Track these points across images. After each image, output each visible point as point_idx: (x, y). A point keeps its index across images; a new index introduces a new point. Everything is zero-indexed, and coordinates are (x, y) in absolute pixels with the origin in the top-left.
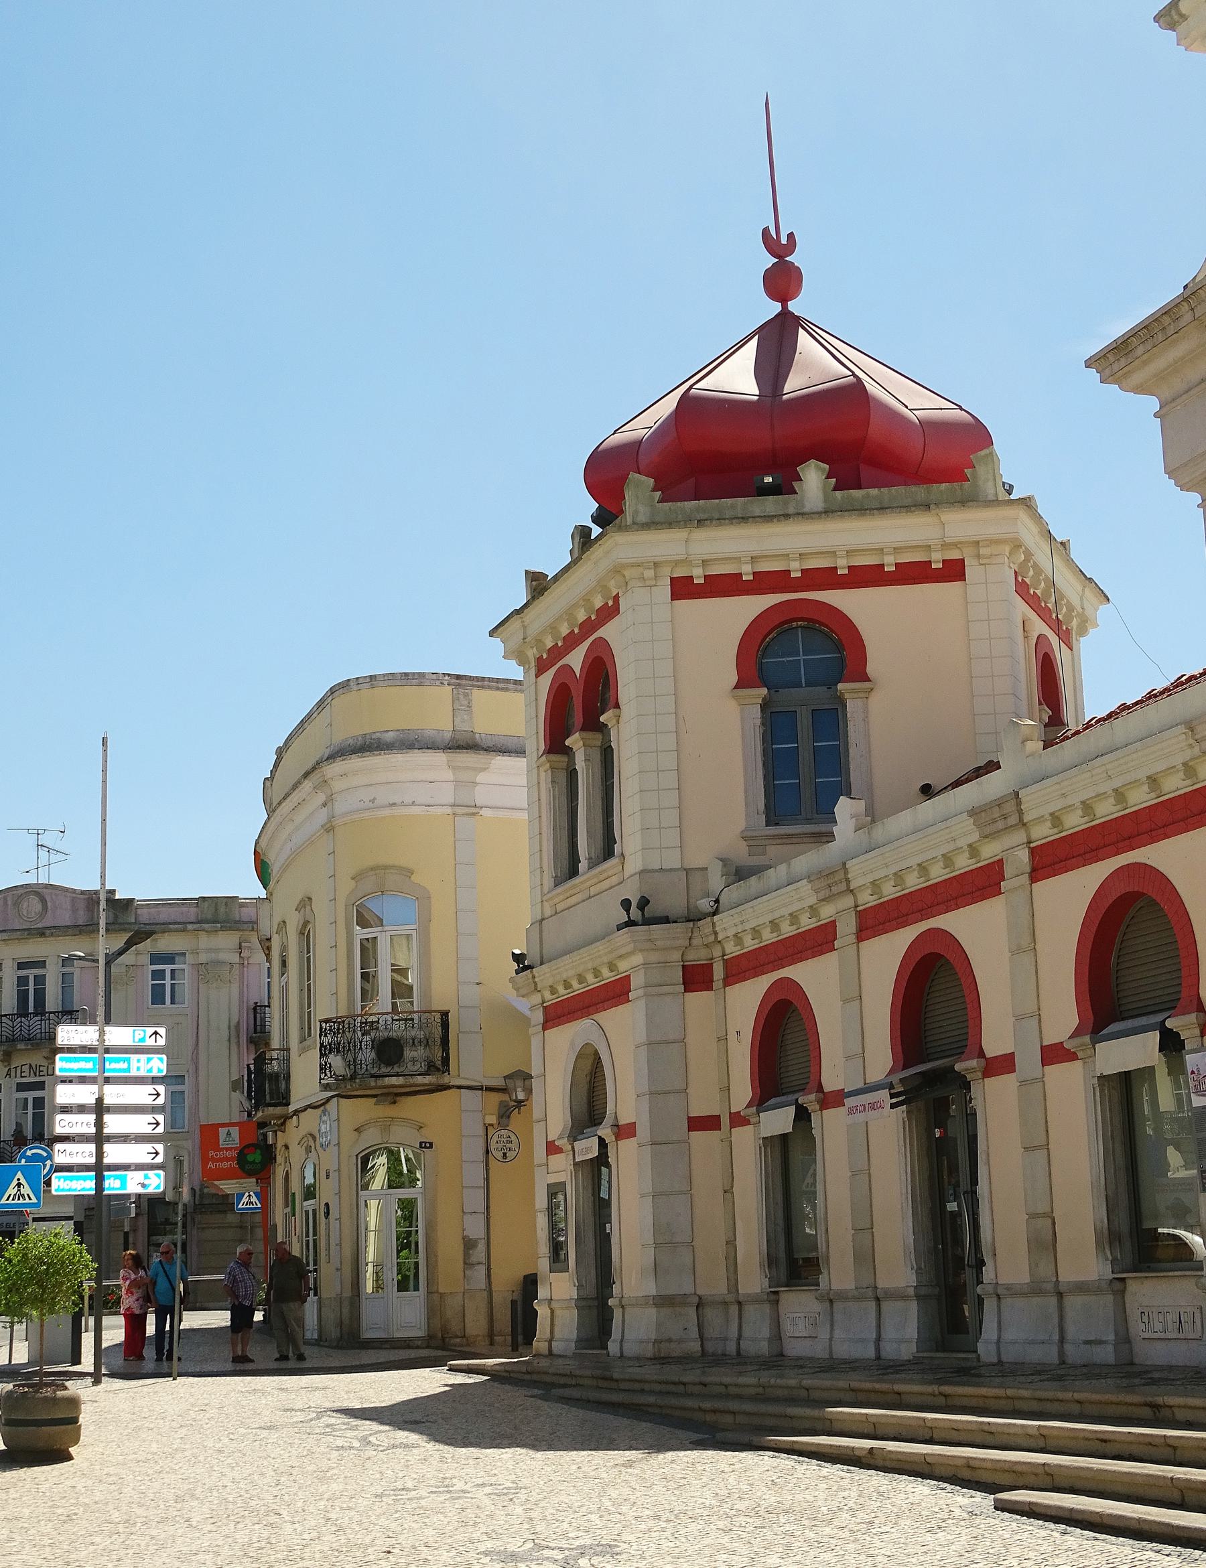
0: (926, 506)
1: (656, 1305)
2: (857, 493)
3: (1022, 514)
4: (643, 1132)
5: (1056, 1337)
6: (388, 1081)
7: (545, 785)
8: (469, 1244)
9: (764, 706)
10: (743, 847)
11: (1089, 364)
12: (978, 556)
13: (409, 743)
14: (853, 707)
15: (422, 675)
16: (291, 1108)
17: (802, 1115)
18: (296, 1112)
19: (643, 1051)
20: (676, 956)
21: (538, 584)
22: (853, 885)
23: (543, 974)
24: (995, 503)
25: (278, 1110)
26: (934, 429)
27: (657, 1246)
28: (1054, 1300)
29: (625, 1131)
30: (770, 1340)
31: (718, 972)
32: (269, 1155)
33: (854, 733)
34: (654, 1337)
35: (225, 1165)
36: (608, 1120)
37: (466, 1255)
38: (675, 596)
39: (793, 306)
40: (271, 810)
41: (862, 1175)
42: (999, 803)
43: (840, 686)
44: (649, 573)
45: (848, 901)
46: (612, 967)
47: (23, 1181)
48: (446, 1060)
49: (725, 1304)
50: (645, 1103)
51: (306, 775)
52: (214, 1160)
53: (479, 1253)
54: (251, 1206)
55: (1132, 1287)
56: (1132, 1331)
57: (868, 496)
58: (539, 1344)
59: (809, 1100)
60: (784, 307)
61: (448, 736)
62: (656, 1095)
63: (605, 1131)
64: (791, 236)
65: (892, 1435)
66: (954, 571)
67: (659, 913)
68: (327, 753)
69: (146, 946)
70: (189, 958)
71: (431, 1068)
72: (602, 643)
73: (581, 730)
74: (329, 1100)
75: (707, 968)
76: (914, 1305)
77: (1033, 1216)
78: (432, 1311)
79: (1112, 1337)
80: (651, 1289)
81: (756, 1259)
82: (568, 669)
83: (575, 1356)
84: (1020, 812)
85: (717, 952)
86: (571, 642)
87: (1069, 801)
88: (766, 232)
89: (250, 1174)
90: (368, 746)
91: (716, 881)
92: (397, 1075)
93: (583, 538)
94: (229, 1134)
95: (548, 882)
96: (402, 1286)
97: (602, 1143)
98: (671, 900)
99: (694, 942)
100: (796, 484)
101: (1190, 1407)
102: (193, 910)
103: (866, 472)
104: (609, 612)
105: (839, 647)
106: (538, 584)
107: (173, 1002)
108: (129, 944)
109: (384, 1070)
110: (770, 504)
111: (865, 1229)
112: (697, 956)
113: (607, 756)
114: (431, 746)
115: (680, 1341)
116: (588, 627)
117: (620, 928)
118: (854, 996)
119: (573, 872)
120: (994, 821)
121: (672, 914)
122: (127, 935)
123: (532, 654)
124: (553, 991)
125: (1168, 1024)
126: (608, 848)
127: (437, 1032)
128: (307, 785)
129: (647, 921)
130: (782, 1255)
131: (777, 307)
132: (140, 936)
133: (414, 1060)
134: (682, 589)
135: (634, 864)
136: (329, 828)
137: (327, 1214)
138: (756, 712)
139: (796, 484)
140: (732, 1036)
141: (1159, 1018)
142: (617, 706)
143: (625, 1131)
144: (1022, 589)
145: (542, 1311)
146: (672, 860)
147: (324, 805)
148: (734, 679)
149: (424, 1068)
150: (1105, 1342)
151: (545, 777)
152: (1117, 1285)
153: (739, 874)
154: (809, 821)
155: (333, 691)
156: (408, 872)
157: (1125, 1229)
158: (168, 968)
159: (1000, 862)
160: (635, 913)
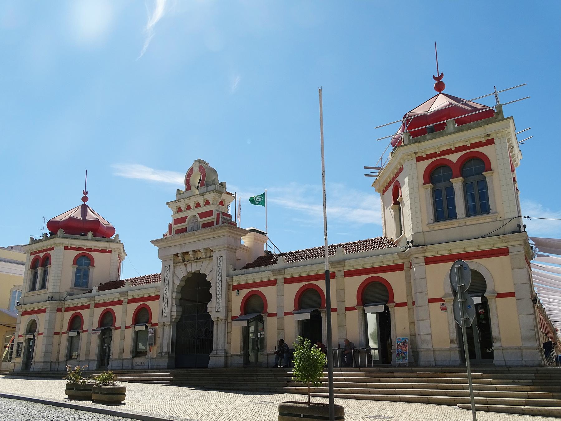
1: (43, 363)
3: (121, 245)
5: (122, 366)
11: (154, 242)
12: (114, 250)
17: (78, 333)
19: (48, 321)
20: (56, 306)
22: (95, 300)
26: (108, 228)
27: (45, 353)
28: (122, 361)
30: (131, 366)
31: (63, 309)
33: (90, 274)
34: (42, 368)
38: (65, 249)
39: (86, 203)
41: (89, 343)
43: (90, 267)
49: (55, 362)
50: (47, 330)
55: (135, 359)
56: (134, 364)
57: (98, 238)
59: (80, 331)
60: (85, 203)
64: (87, 192)
66: (110, 252)
73: (41, 267)
76: (96, 362)
79: (131, 365)
80: (43, 360)
87: (136, 294)
88: (84, 191)
97: (34, 336)
98: (57, 297)
100: (87, 235)
101: (516, 373)
110: (83, 237)
113: (45, 273)
115: (47, 369)
117: (46, 301)
118: (92, 316)
120: (123, 295)
121: (420, 245)
123: (30, 252)
126: (43, 286)
129: (52, 300)
130: (69, 354)
131: (83, 203)
134: (66, 248)
139: (87, 235)
140: (64, 320)
141: (145, 324)
144: (119, 256)
146: (58, 291)
150: (130, 366)
152: (133, 358)
153: (70, 294)
154: (81, 287)
157: (134, 351)
160: (50, 299)
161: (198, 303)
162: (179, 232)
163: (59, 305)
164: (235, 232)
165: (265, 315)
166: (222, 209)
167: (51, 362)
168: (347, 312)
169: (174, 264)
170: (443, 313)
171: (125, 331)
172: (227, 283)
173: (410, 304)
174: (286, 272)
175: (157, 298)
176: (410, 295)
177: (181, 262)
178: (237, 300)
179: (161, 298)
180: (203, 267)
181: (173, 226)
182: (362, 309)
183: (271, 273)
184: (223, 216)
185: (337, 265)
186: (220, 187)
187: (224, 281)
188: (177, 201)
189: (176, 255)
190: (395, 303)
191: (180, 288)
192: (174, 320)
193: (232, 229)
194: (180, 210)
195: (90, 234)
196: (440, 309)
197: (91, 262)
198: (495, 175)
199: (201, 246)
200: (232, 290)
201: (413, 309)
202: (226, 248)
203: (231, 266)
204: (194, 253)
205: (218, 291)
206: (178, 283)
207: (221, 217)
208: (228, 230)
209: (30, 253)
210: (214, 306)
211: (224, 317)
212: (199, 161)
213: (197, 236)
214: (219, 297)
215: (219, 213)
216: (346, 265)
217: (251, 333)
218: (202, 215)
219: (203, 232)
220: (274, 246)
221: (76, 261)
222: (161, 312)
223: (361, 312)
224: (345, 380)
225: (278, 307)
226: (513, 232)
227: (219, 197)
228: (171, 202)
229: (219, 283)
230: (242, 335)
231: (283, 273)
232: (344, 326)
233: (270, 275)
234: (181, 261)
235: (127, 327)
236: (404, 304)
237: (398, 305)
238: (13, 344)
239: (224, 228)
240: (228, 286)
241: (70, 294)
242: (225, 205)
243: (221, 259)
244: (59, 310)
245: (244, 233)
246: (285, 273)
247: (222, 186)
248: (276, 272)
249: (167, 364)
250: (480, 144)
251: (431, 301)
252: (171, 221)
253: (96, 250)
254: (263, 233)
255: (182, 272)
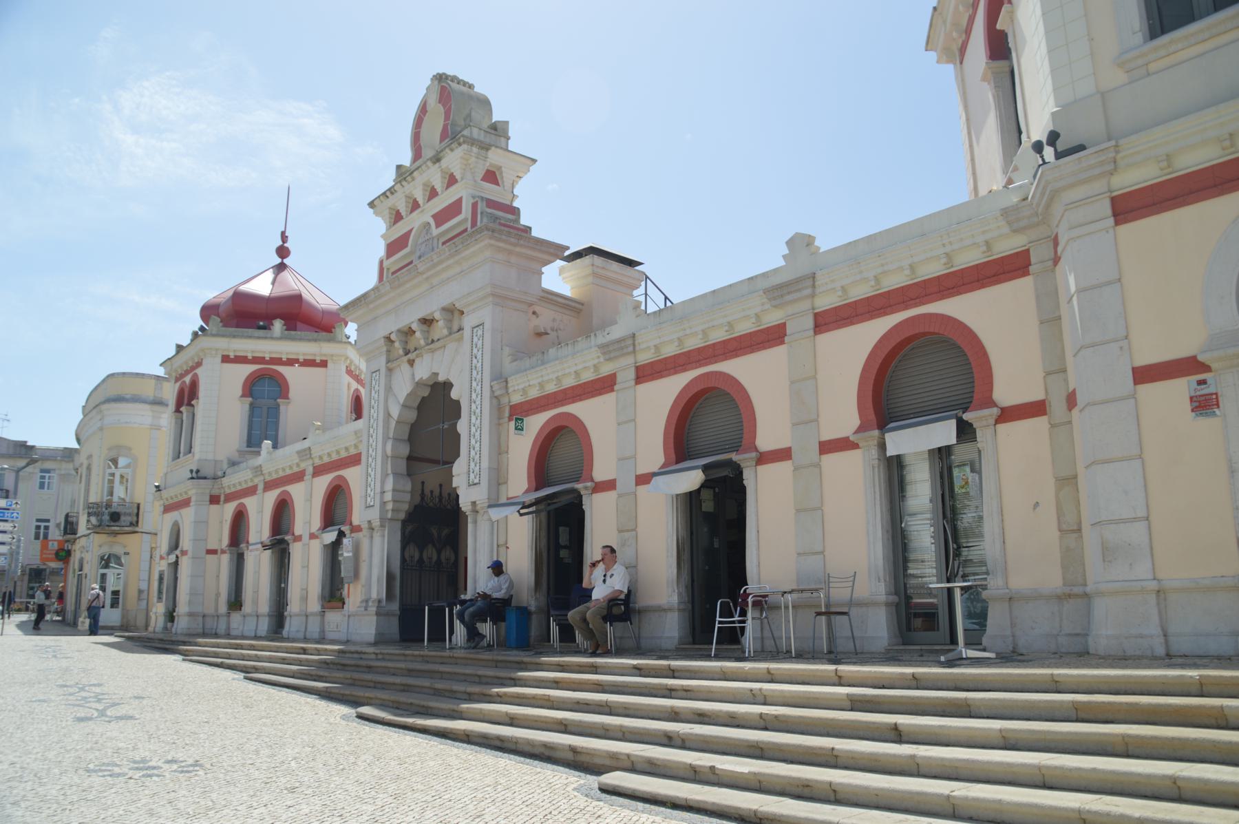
0: (315, 340)
2: (293, 333)
4: (190, 554)
6: (113, 528)
7: (173, 424)
8: (140, 592)
9: (251, 404)
10: (237, 454)
13: (136, 399)
14: (282, 408)
15: (143, 374)
16: (78, 535)
18: (79, 538)
20: (208, 491)
21: (180, 348)
22: (263, 472)
23: (165, 494)
24: (341, 342)
25: (72, 536)
28: (305, 618)
29: (184, 553)
30: (320, 632)
31: (222, 498)
32: (69, 553)
35: (50, 556)
36: (179, 549)
37: (139, 596)
39: (285, 261)
40: (85, 415)
42: (305, 450)
43: (278, 400)
44: (214, 352)
45: (262, 478)
46: (186, 493)
48: (137, 522)
49: (213, 616)
51: (94, 408)
52: (45, 554)
53: (144, 596)
58: (151, 629)
61: (151, 398)
62: (195, 540)
63: (178, 552)
65: (800, 682)
66: (324, 364)
67: (203, 475)
68: (103, 399)
69: (38, 465)
70: (57, 472)
71: (131, 524)
72: (196, 375)
74: (90, 534)
75: (218, 497)
76: (676, 614)
77: (302, 589)
78: (123, 616)
81: (316, 597)
82: (184, 382)
83: (162, 633)
84: (311, 454)
85: (223, 491)
86: (187, 372)
89: (60, 560)
90: (119, 399)
91: (225, 466)
92: (117, 526)
93: (195, 335)
94: (53, 544)
95: (170, 459)
96: (112, 606)
97: (177, 557)
99: (215, 487)
102: (61, 452)
103: (299, 325)
104: (199, 364)
105: (279, 386)
106: (180, 348)
107: (48, 489)
108: (28, 465)
109: (112, 524)
110: (261, 333)
111: (256, 592)
112: (215, 492)
114: (144, 402)
116: (193, 368)
119: (179, 457)
122: (28, 460)
123: (174, 374)
124: (167, 499)
125: (342, 529)
126: (190, 450)
127: (136, 511)
128: (94, 412)
129: (199, 478)
132: (33, 461)
133: (124, 521)
134: (226, 359)
135: (197, 457)
136: (101, 429)
137: (86, 577)
138: (247, 407)
142: (198, 399)
143: (184, 553)
145: (153, 617)
146: (210, 457)
147: (100, 420)
148: (240, 393)
149: (128, 524)
151: (173, 421)
152: (322, 613)
155: (108, 376)
156: (130, 449)
158: (47, 475)
159: (305, 470)
160: (194, 475)
161: (443, 465)
163: (213, 488)
164: (518, 249)
165: (586, 488)
166: (491, 191)
167: (204, 616)
168: (825, 458)
169: (387, 363)
170: (1207, 425)
171: (308, 544)
172: (495, 401)
173: (1057, 406)
174: (639, 344)
175: (355, 460)
176: (1056, 370)
177: (402, 356)
178: (521, 448)
179: (364, 459)
181: (386, 264)
182: (876, 442)
183: (600, 354)
184: (489, 210)
185: (789, 293)
186: (488, 135)
187: (487, 393)
188: (388, 194)
190: (996, 406)
191: (407, 429)
192: (389, 516)
193: (504, 237)
194: (397, 217)
195: (278, 325)
196: (1187, 406)
197: (281, 388)
199: (432, 306)
200: (507, 419)
201: (1070, 422)
202: (491, 299)
203: (507, 350)
204: (425, 327)
205: (474, 426)
206: (395, 412)
207: (482, 213)
208: (493, 242)
209: (174, 378)
210: (465, 470)
211: (487, 501)
212: (440, 78)
213: (425, 276)
214: (476, 442)
215: (477, 202)
216: (818, 291)
217: (565, 547)
218: (440, 218)
219: (435, 261)
220: (666, 298)
221: (251, 387)
222: (364, 494)
223: (874, 452)
224: (914, 682)
225: (619, 460)
227: (477, 158)
228: (378, 200)
229: (475, 402)
230: (532, 550)
231: (631, 349)
232: (814, 509)
233: (596, 362)
234: (401, 352)
236: (1036, 409)
237: (1009, 414)
238: (80, 573)
239: (479, 236)
240: (497, 407)
241: (233, 464)
242: (503, 182)
243: (480, 332)
244: (214, 500)
245: (551, 254)
246: (637, 348)
247: (495, 133)
248: (611, 348)
249: (373, 631)
251: (1144, 375)
252: (381, 252)
253: (291, 362)
254: (631, 263)
255: (403, 386)
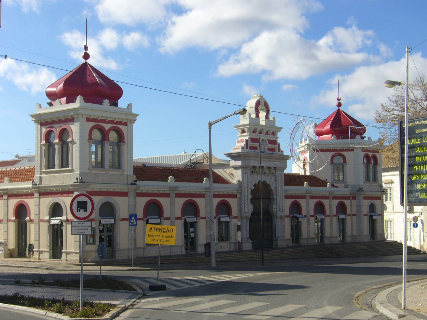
47: (134, 219)
54: (134, 224)
162: (251, 148)
180: (268, 179)
189: (254, 167)
198: (126, 146)
226: (131, 184)
235: (177, 218)
250: (342, 150)
255: (256, 179)
